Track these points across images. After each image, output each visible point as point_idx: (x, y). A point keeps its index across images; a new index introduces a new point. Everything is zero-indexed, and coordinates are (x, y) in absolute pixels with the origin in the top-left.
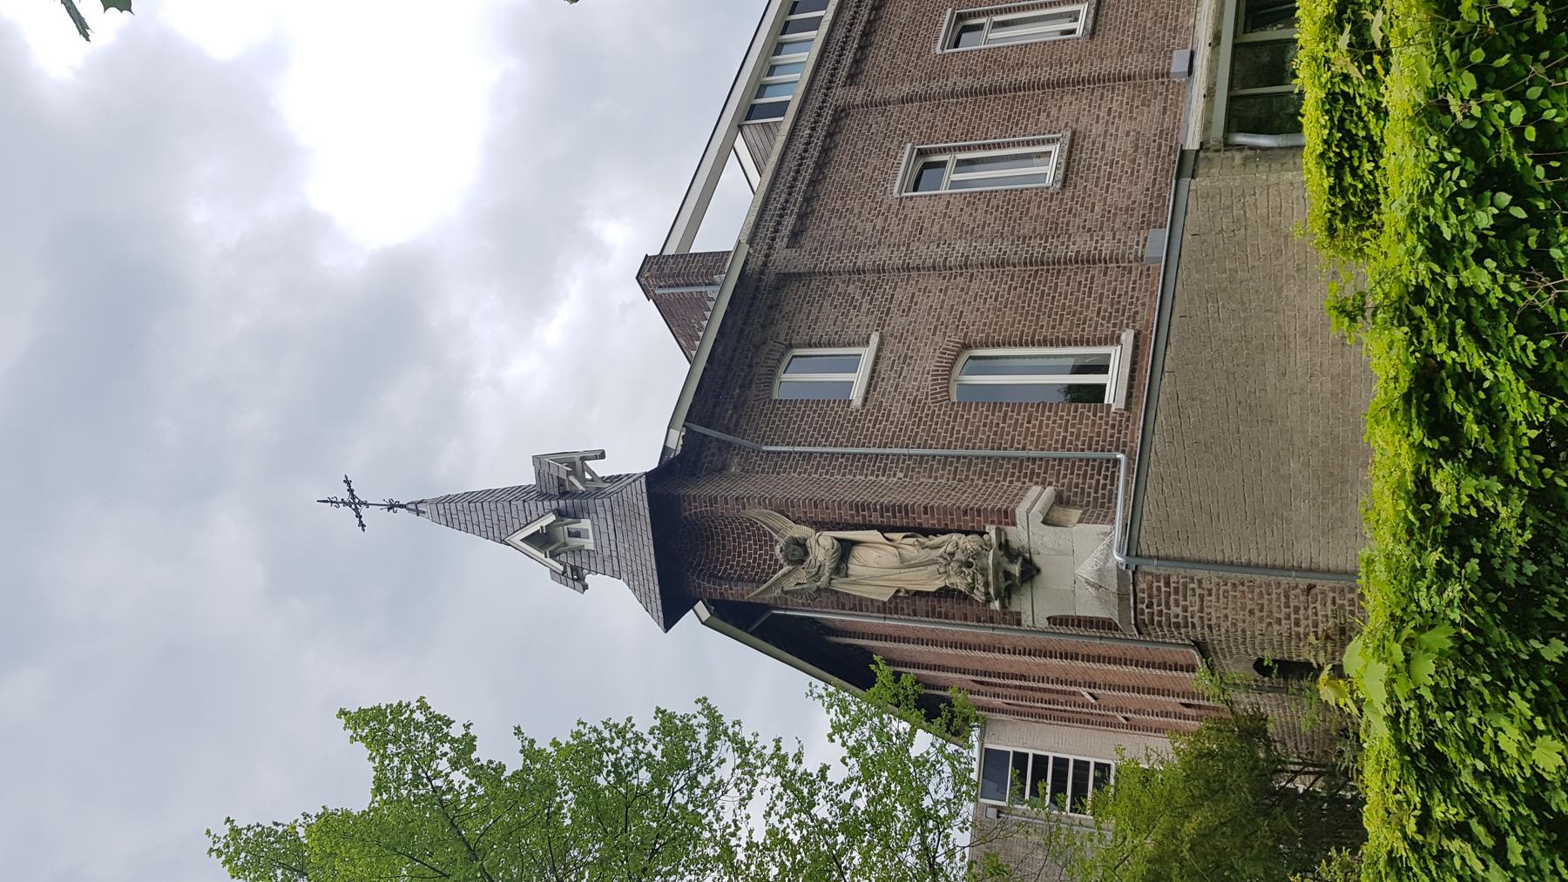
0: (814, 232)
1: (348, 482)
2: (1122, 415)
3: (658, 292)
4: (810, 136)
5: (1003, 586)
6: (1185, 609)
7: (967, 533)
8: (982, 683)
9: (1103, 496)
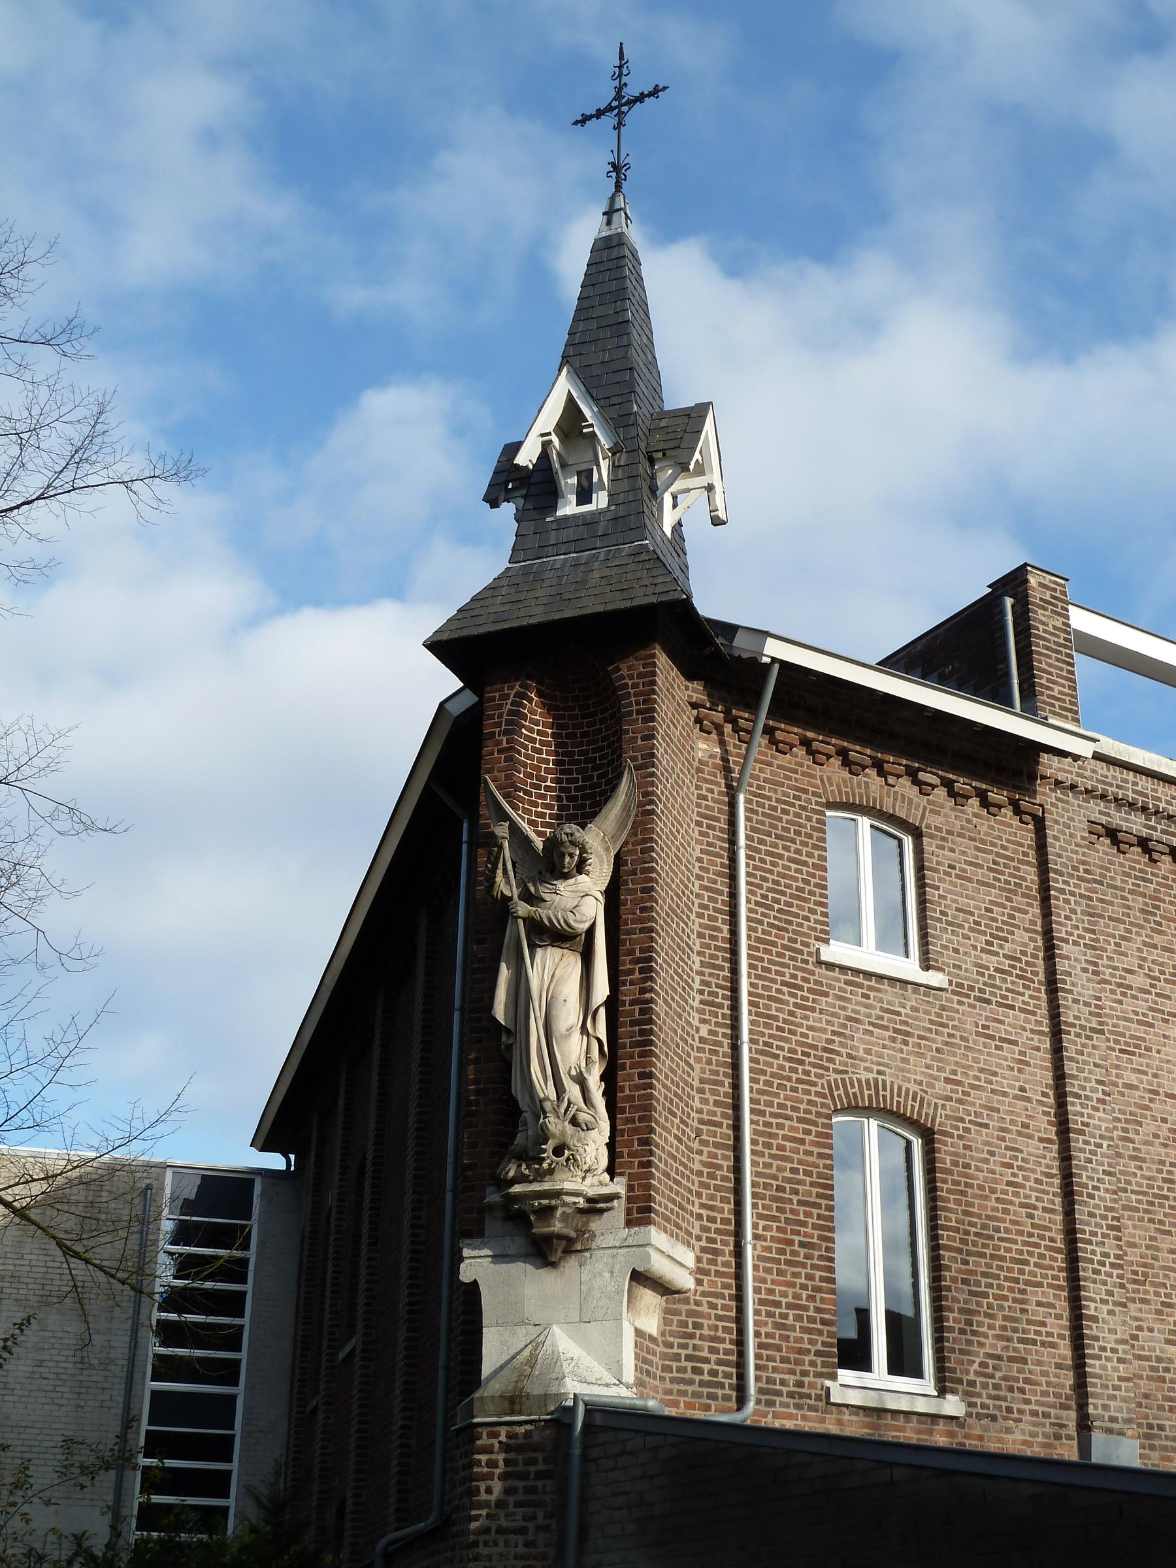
1: (655, 92)
7: (611, 1146)
8: (362, 1170)
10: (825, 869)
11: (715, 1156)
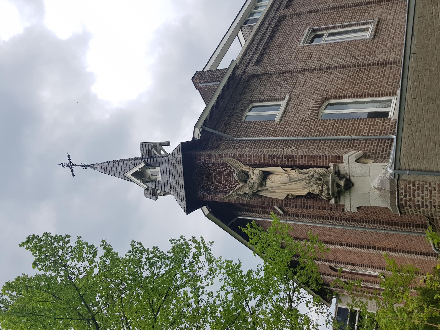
0: (266, 60)
3: (200, 85)
4: (268, 27)
5: (336, 190)
6: (423, 198)
9: (386, 154)
10: (256, 121)
11: (327, 146)
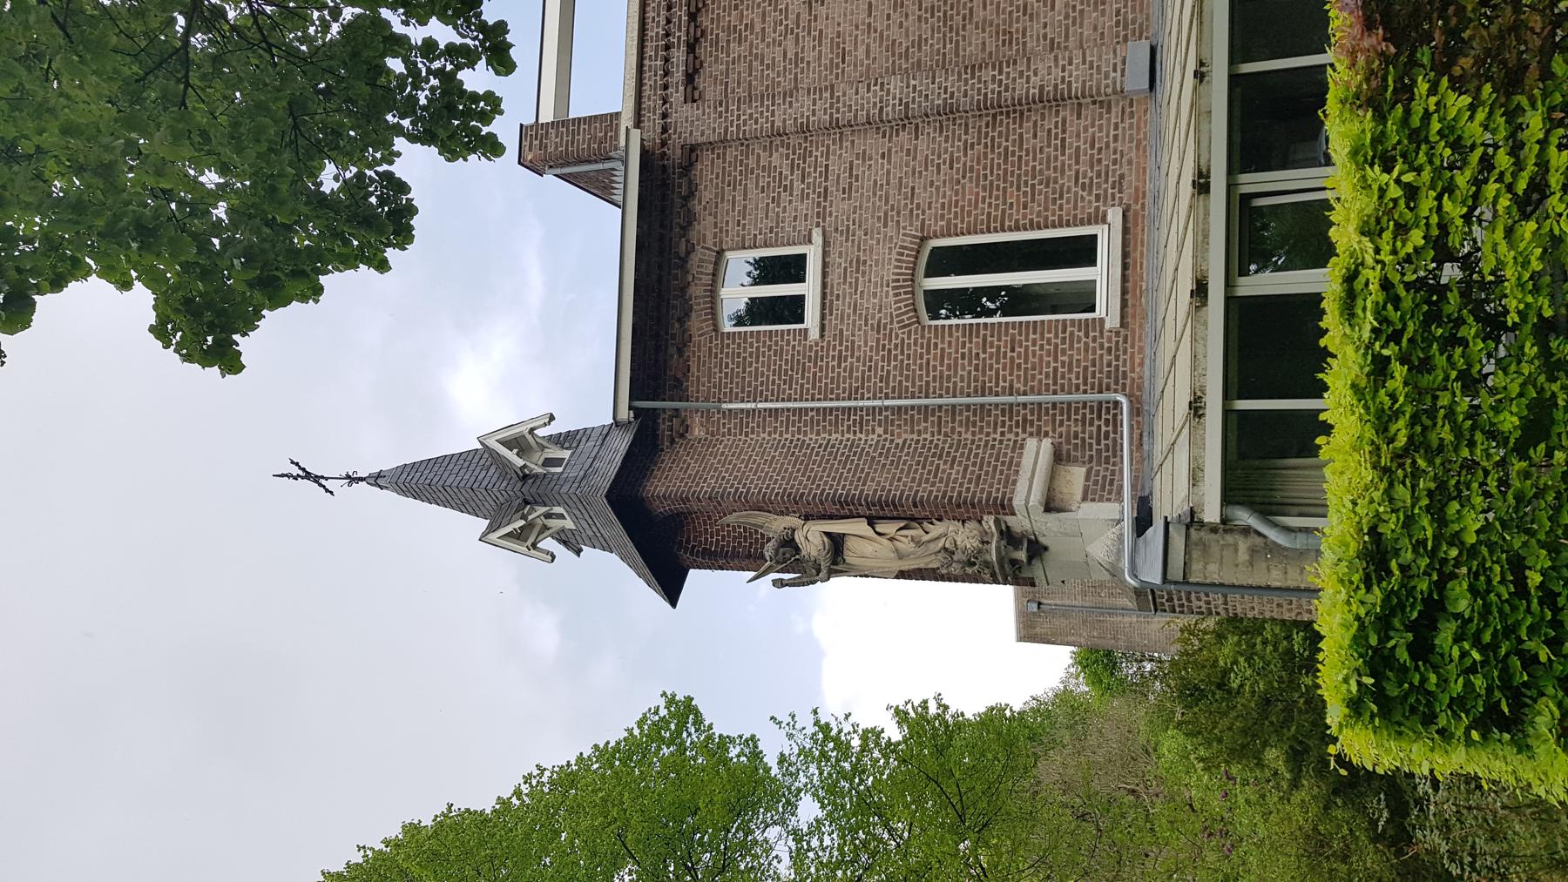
0: (712, 67)
2: (1118, 334)
6: (1208, 603)
